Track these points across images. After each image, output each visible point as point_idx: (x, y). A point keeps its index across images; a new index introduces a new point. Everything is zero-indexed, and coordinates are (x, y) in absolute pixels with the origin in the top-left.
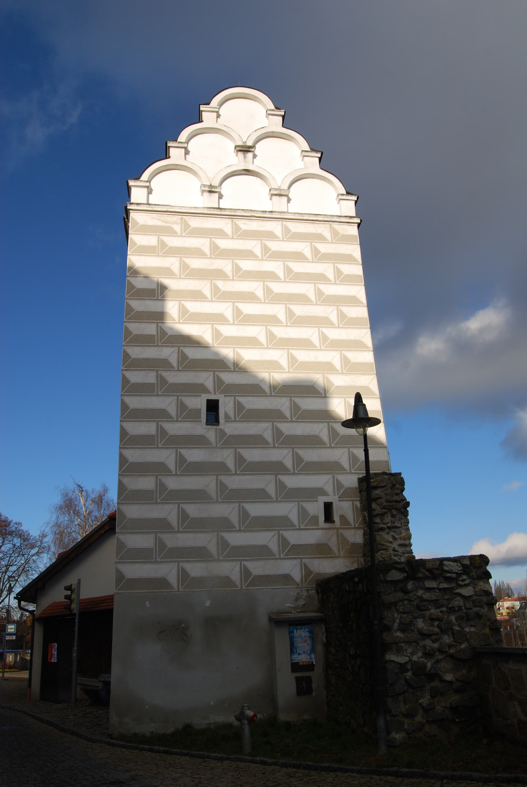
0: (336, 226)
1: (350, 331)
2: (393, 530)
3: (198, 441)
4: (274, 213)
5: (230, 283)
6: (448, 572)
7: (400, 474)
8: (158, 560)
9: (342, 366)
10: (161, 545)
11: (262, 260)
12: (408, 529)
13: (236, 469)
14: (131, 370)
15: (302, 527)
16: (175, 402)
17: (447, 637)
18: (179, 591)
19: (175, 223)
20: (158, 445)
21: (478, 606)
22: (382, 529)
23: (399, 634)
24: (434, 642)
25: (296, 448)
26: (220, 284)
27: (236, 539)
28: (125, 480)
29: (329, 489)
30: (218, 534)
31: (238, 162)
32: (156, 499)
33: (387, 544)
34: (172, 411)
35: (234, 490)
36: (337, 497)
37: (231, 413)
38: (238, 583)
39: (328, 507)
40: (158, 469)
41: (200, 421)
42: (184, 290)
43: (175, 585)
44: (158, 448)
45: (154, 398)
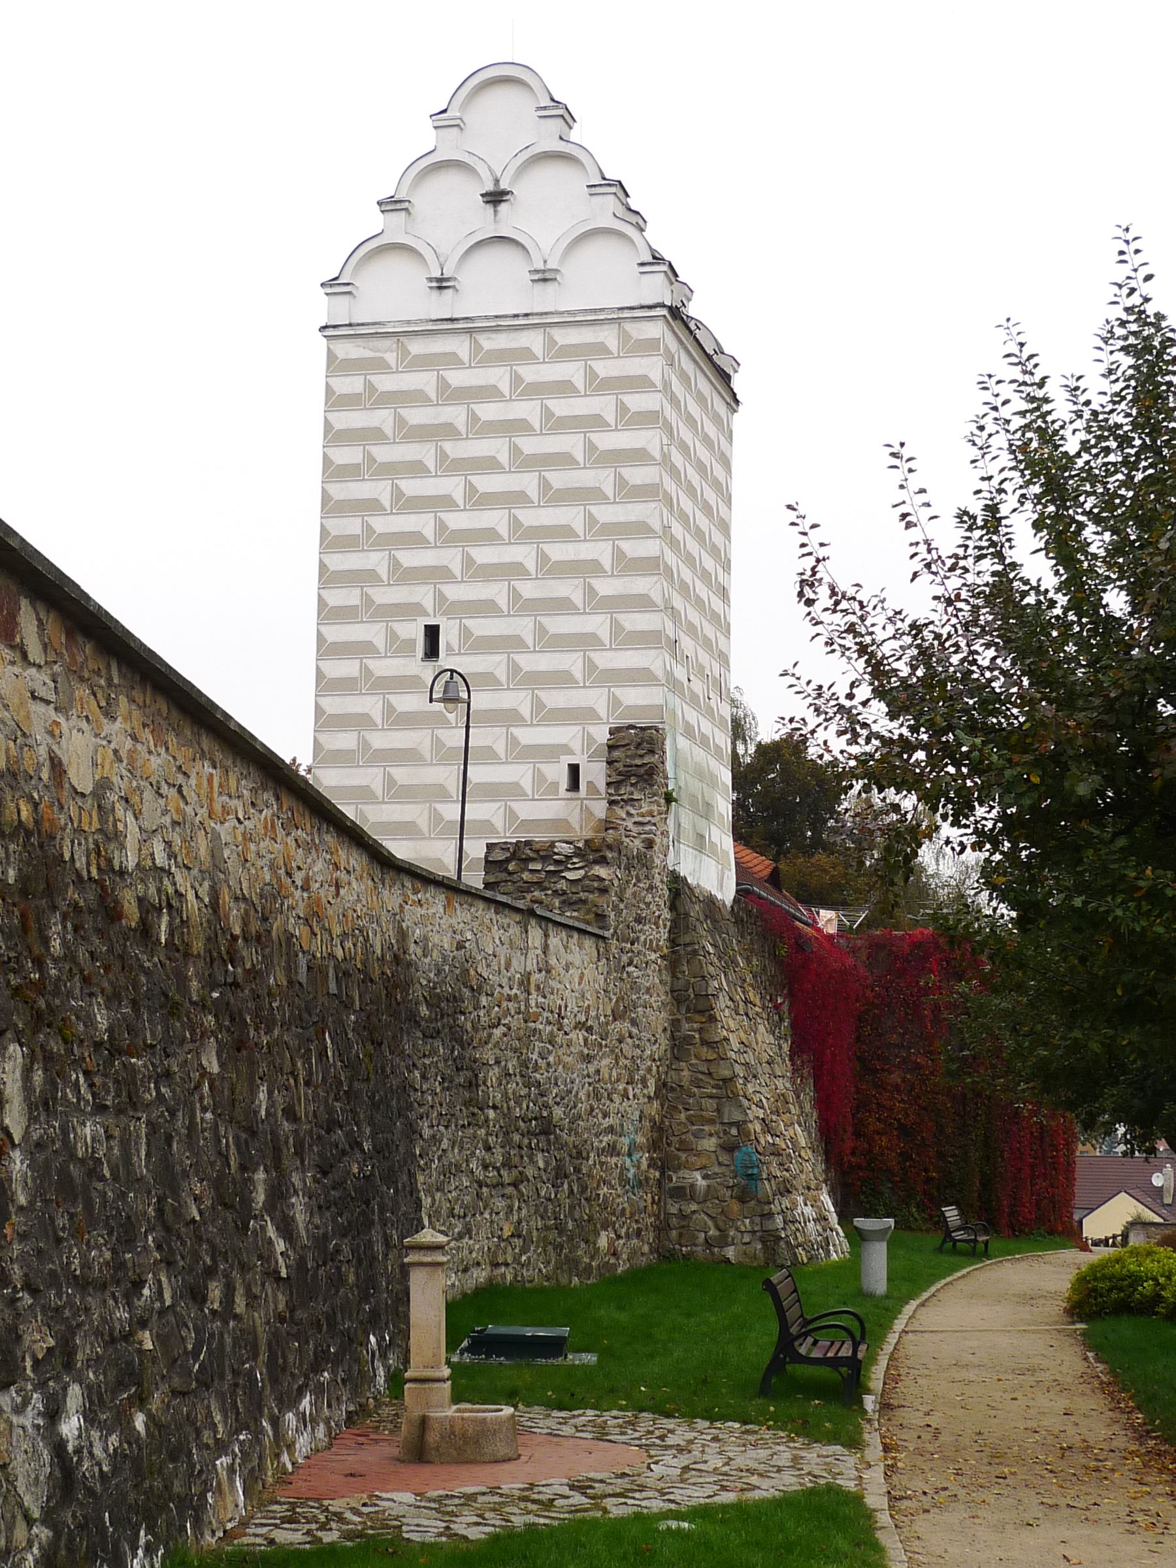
19: (390, 350)
28: (322, 738)
29: (576, 746)
31: (483, 222)
39: (574, 770)
40: (362, 722)
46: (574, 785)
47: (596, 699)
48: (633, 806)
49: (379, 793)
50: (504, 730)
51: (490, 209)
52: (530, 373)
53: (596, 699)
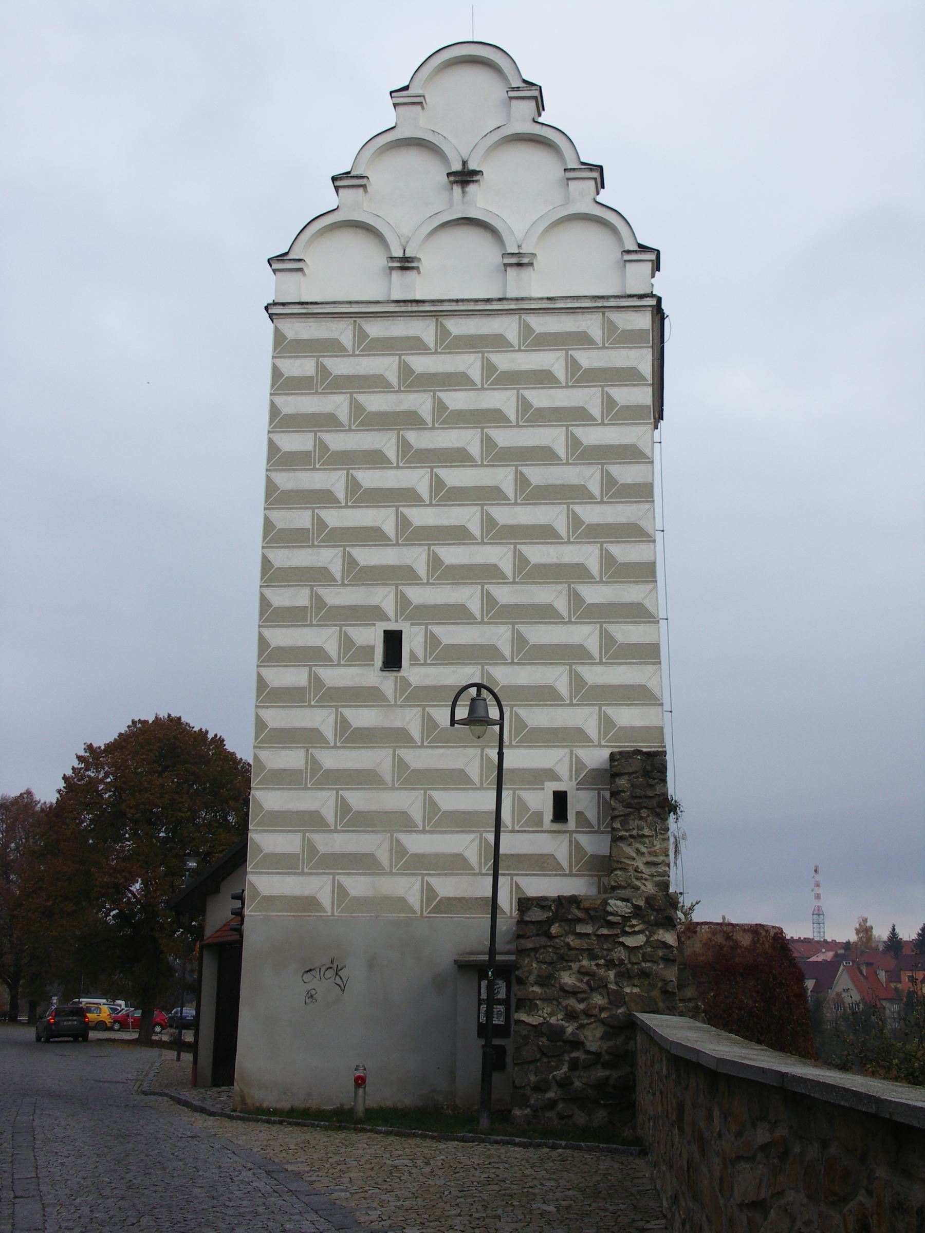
1: (619, 507)
3: (367, 696)
5: (427, 434)
6: (612, 914)
8: (306, 870)
9: (601, 570)
11: (482, 389)
15: (517, 828)
16: (337, 634)
17: (599, 997)
18: (333, 915)
20: (310, 702)
21: (648, 961)
23: (536, 989)
24: (580, 1001)
25: (516, 705)
26: (412, 436)
27: (417, 843)
30: (392, 836)
32: (306, 784)
33: (626, 861)
34: (332, 649)
36: (574, 783)
37: (420, 653)
38: (417, 907)
39: (560, 799)
41: (373, 665)
42: (356, 451)
43: (328, 907)
44: (310, 706)
45: (306, 630)
47: (586, 718)
48: (644, 843)
51: (457, 189)
52: (503, 361)
53: (586, 718)
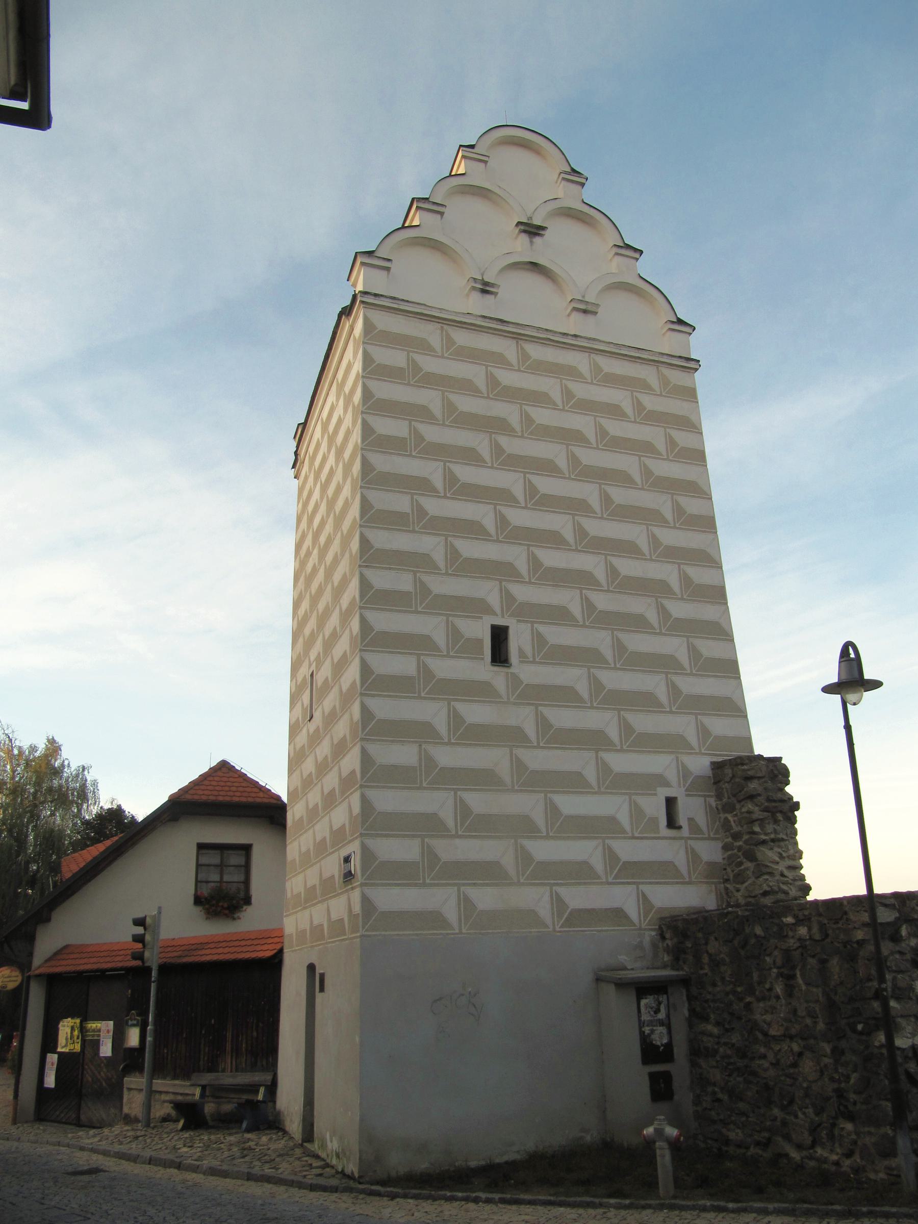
0: (665, 371)
2: (777, 843)
3: (478, 691)
4: (579, 339)
7: (781, 758)
10: (430, 855)
12: (796, 843)
13: (538, 739)
14: (374, 567)
18: (461, 933)
22: (764, 842)
31: (521, 248)
35: (537, 772)
36: (683, 789)
37: (528, 649)
39: (670, 803)
40: (421, 732)
41: (483, 659)
43: (455, 924)
46: (672, 823)
49: (450, 823)
50: (507, 750)
53: (683, 725)
